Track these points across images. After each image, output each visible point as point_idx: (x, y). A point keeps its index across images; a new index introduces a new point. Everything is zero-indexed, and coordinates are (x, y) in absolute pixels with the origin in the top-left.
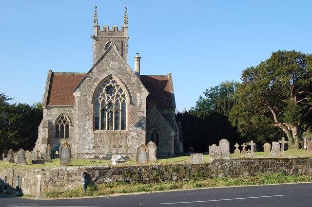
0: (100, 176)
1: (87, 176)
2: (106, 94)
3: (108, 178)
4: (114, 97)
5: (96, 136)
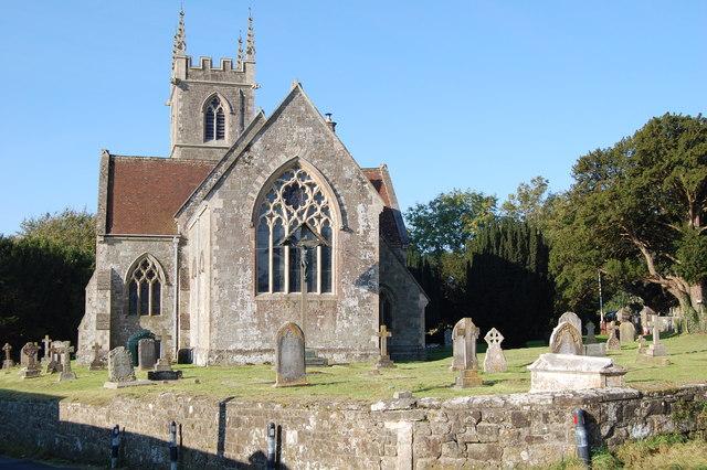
0: (620, 420)
1: (588, 421)
2: (283, 206)
3: (640, 426)
4: (303, 212)
5: (262, 307)
